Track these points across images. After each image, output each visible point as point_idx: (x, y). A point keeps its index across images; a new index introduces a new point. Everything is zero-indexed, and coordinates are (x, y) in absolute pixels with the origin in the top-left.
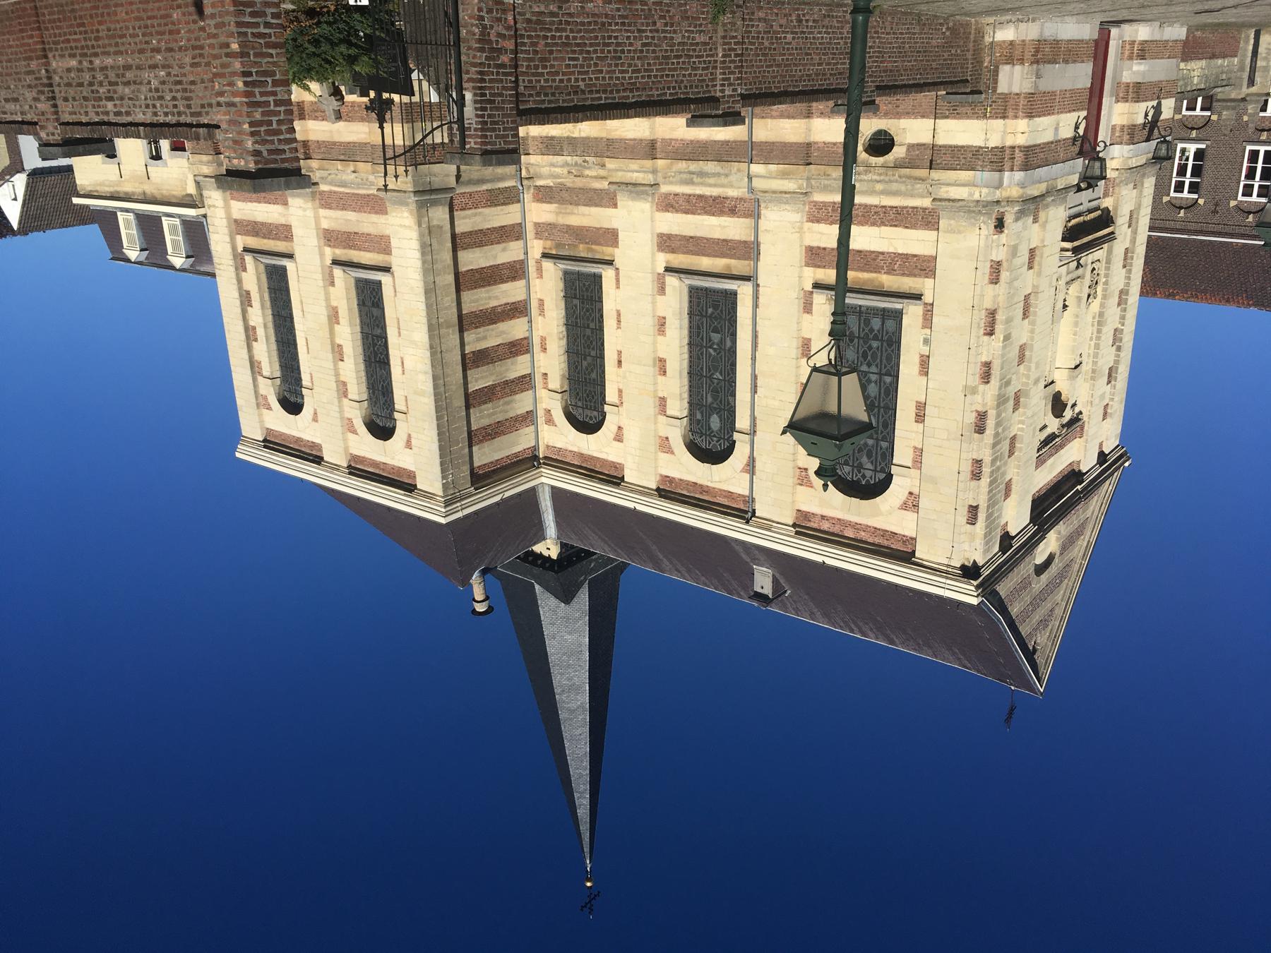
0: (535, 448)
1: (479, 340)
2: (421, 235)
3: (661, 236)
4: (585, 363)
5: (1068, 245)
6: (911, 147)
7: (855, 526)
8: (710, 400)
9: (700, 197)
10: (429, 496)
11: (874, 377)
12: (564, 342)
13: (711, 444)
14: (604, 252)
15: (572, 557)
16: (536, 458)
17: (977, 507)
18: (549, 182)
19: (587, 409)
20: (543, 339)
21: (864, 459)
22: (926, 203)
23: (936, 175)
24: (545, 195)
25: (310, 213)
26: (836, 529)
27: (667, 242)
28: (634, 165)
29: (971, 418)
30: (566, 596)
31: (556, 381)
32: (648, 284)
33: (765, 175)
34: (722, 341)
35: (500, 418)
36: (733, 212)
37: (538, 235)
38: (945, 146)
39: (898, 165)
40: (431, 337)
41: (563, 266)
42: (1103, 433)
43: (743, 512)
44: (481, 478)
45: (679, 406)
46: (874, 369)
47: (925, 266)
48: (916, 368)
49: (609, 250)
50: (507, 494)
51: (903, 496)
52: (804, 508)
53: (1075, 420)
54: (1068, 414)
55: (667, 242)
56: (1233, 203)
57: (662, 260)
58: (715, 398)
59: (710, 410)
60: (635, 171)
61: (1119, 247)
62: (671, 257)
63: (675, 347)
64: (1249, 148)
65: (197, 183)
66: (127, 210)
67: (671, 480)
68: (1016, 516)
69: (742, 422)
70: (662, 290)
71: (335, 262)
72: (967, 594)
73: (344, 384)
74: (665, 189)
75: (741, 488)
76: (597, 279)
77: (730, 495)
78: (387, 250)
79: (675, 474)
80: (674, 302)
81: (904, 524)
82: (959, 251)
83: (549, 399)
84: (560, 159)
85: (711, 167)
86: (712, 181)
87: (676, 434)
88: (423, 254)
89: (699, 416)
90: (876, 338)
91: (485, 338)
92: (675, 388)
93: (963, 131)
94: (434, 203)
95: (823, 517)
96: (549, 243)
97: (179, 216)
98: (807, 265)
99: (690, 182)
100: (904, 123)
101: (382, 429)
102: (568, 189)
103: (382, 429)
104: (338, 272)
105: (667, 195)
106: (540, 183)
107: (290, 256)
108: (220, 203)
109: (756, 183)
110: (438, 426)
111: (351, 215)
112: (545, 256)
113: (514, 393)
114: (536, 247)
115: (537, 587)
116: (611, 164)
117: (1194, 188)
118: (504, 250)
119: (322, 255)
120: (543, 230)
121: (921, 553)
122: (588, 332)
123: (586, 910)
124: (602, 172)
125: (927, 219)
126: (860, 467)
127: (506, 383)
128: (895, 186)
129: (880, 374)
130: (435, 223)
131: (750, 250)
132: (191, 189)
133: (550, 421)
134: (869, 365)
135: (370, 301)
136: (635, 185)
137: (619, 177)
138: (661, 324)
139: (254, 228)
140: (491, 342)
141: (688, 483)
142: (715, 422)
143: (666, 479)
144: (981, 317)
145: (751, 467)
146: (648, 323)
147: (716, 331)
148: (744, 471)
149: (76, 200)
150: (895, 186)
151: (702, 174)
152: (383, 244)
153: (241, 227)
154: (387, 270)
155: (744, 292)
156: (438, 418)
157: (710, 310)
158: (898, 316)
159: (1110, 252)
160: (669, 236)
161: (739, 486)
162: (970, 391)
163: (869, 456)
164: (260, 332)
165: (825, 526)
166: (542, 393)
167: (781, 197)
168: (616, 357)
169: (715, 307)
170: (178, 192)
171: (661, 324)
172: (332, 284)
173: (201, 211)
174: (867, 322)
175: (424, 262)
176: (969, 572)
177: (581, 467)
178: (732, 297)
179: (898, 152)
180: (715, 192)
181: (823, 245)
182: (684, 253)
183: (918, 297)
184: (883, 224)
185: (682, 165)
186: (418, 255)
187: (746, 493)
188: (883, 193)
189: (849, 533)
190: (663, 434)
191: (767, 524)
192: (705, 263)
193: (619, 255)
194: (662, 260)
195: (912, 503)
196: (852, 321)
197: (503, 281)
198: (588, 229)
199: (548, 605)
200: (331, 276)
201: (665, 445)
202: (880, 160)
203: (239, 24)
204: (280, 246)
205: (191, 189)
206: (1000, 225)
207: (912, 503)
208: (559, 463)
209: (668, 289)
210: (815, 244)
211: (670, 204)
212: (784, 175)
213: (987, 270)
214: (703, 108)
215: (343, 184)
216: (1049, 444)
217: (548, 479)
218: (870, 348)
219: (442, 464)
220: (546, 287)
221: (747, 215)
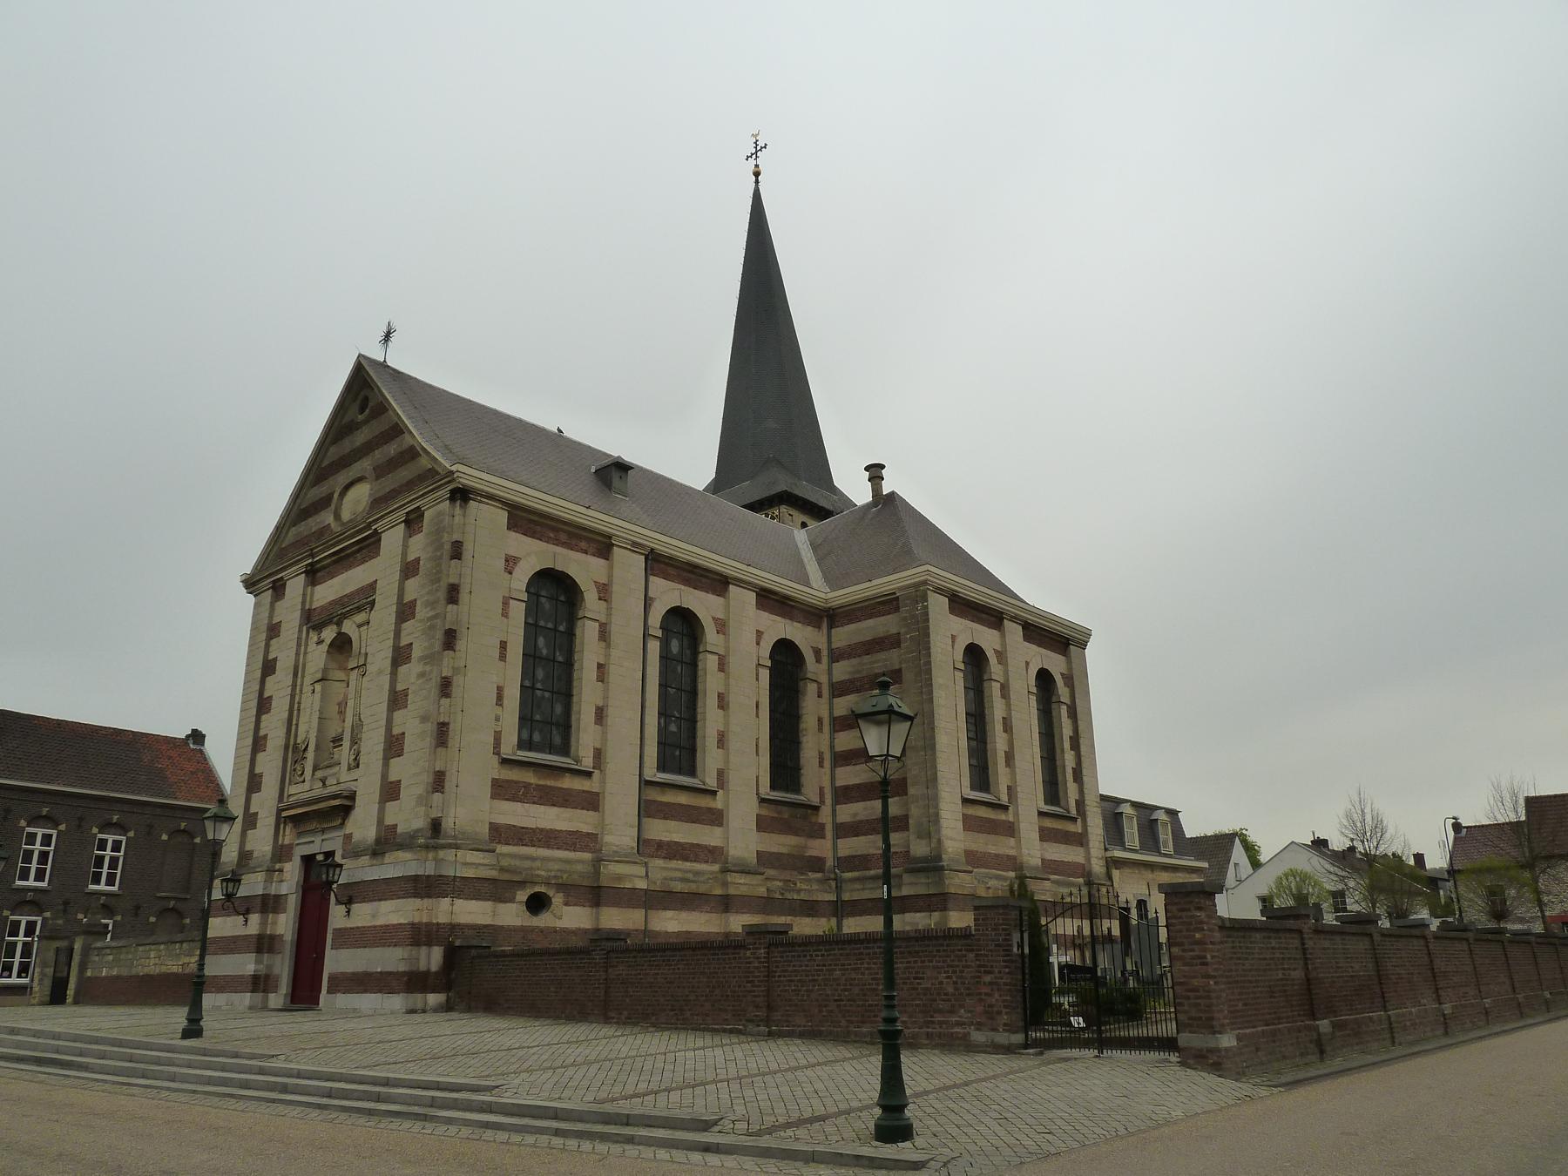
0: (830, 627)
2: (938, 831)
3: (720, 825)
6: (512, 900)
9: (686, 859)
12: (802, 726)
17: (453, 558)
18: (812, 875)
20: (820, 730)
22: (502, 849)
23: (493, 874)
24: (816, 864)
25: (1025, 851)
27: (716, 818)
28: (743, 890)
29: (461, 645)
31: (811, 688)
32: (734, 779)
33: (635, 877)
35: (866, 659)
36: (660, 845)
37: (822, 826)
39: (522, 884)
40: (933, 738)
44: (888, 604)
47: (500, 790)
48: (506, 693)
49: (764, 812)
51: (517, 572)
52: (602, 561)
54: (329, 634)
56: (131, 834)
60: (741, 885)
62: (712, 804)
63: (711, 720)
64: (115, 888)
65: (1110, 878)
66: (1166, 855)
69: (654, 647)
70: (721, 774)
71: (1005, 808)
73: (1003, 696)
74: (716, 867)
75: (657, 583)
76: (774, 786)
78: (966, 818)
79: (711, 597)
80: (710, 760)
81: (520, 544)
82: (472, 807)
84: (803, 896)
85: (678, 887)
86: (679, 875)
87: (711, 636)
88: (937, 815)
92: (711, 681)
93: (471, 912)
94: (925, 859)
96: (813, 819)
97: (1125, 849)
98: (597, 794)
99: (697, 873)
100: (518, 922)
101: (974, 654)
103: (974, 654)
104: (1004, 799)
105: (715, 862)
106: (819, 875)
107: (1041, 814)
108: (1094, 861)
109: (642, 871)
110: (929, 655)
111: (992, 850)
112: (816, 809)
113: (851, 681)
114: (825, 816)
116: (762, 891)
117: (102, 845)
118: (855, 815)
119: (1016, 814)
120: (818, 832)
121: (502, 516)
123: (761, 144)
124: (769, 884)
125: (500, 833)
127: (858, 691)
128: (527, 864)
130: (924, 842)
131: (647, 809)
132: (1116, 873)
133: (817, 652)
135: (981, 775)
136: (742, 872)
137: (756, 879)
139: (992, 828)
144: (453, 741)
146: (734, 744)
149: (1206, 865)
150: (527, 864)
151: (683, 880)
152: (970, 824)
153: (1080, 840)
154: (966, 801)
155: (651, 773)
158: (524, 744)
164: (1067, 745)
165: (583, 544)
166: (824, 679)
170: (1127, 871)
171: (722, 741)
172: (1009, 788)
173: (1109, 854)
175: (936, 807)
178: (662, 767)
179: (522, 896)
180: (674, 864)
183: (505, 762)
185: (702, 889)
186: (943, 814)
187: (652, 578)
188: (533, 859)
192: (683, 799)
193: (495, 771)
195: (511, 563)
196: (557, 740)
197: (858, 786)
198: (781, 832)
200: (1010, 795)
201: (722, 626)
202: (537, 889)
203: (1209, 997)
204: (1048, 823)
205: (1116, 873)
207: (511, 563)
209: (715, 774)
210: (591, 813)
211: (713, 854)
212: (620, 878)
213: (447, 785)
214: (775, 939)
215: (998, 877)
219: (927, 620)
220: (815, 779)
221: (648, 842)
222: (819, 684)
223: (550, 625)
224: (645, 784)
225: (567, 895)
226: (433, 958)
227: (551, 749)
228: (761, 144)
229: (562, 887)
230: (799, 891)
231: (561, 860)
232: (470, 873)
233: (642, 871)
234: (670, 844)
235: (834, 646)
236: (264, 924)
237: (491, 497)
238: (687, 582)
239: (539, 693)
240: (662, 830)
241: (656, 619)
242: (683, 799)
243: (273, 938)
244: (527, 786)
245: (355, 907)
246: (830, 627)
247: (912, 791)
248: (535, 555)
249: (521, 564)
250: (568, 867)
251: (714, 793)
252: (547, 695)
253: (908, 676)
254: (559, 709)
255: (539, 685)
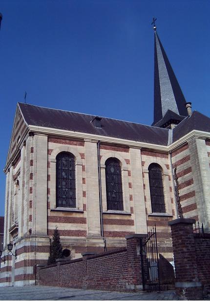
0: (171, 157)
1: (189, 189)
3: (133, 225)
4: (157, 185)
5: (17, 227)
7: (66, 143)
8: (114, 177)
10: (201, 138)
11: (64, 187)
13: (113, 163)
14: (150, 219)
15: (167, 125)
16: (171, 154)
19: (155, 172)
21: (65, 163)
26: (72, 142)
30: (169, 112)
34: (112, 194)
36: (110, 233)
38: (46, 252)
40: (202, 188)
41: (76, 209)
42: (9, 177)
43: (144, 150)
44: (185, 145)
45: (78, 169)
46: (64, 189)
48: (51, 190)
50: (178, 141)
53: (15, 180)
55: (131, 223)
57: (85, 215)
58: (113, 177)
59: (114, 174)
61: (8, 228)
63: (126, 192)
67: (125, 151)
68: (24, 151)
69: (103, 171)
70: (84, 206)
72: (32, 128)
76: (153, 211)
77: (106, 149)
79: (123, 153)
80: (127, 205)
83: (168, 172)
86: (118, 242)
87: (124, 165)
89: (118, 171)
90: (64, 198)
91: (188, 189)
95: (76, 145)
102: (165, 237)
110: (198, 160)
115: (179, 114)
122: (156, 194)
123: (155, 19)
126: (66, 161)
129: (62, 188)
131: (103, 222)
133: (167, 166)
134: (65, 190)
138: (131, 198)
140: (186, 188)
141: (120, 151)
142: (112, 170)
143: (127, 151)
145: (99, 157)
147: (114, 197)
148: (102, 156)
155: (105, 210)
156: (198, 163)
157: (116, 203)
159: (10, 226)
160: (130, 225)
161: (52, 145)
162: (35, 185)
163: (64, 164)
165: (75, 143)
167: (94, 237)
168: (146, 187)
169: (114, 204)
171: (131, 198)
174: (67, 203)
176: (32, 134)
177: (156, 152)
180: (116, 238)
181: (81, 224)
182: (125, 220)
184: (64, 231)
187: (142, 155)
189: (67, 141)
190: (128, 165)
191: (93, 141)
192: (118, 217)
194: (85, 215)
195: (49, 152)
199: (175, 109)
206: (30, 231)
207: (143, 163)
208: (164, 154)
212: (94, 244)
216: (19, 173)
217: (167, 148)
218: (65, 195)
222: (169, 176)
223: (66, 168)
224: (102, 214)
225: (76, 250)
226: (30, 270)
227: (70, 206)
228: (155, 19)
229: (74, 247)
230: (166, 244)
231: (74, 239)
232: (40, 245)
233: (103, 241)
234: (114, 232)
235: (173, 163)
236: (8, 263)
237: (41, 133)
238: (114, 150)
239: (64, 189)
240: (109, 228)
241: (103, 162)
242: (118, 217)
243: (10, 267)
244: (60, 217)
245: (18, 257)
246: (171, 157)
247: (198, 207)
248: (57, 148)
249: (54, 151)
250: (76, 242)
251: (130, 215)
252: (67, 189)
253: (193, 169)
254: (109, 194)
255: (64, 187)
